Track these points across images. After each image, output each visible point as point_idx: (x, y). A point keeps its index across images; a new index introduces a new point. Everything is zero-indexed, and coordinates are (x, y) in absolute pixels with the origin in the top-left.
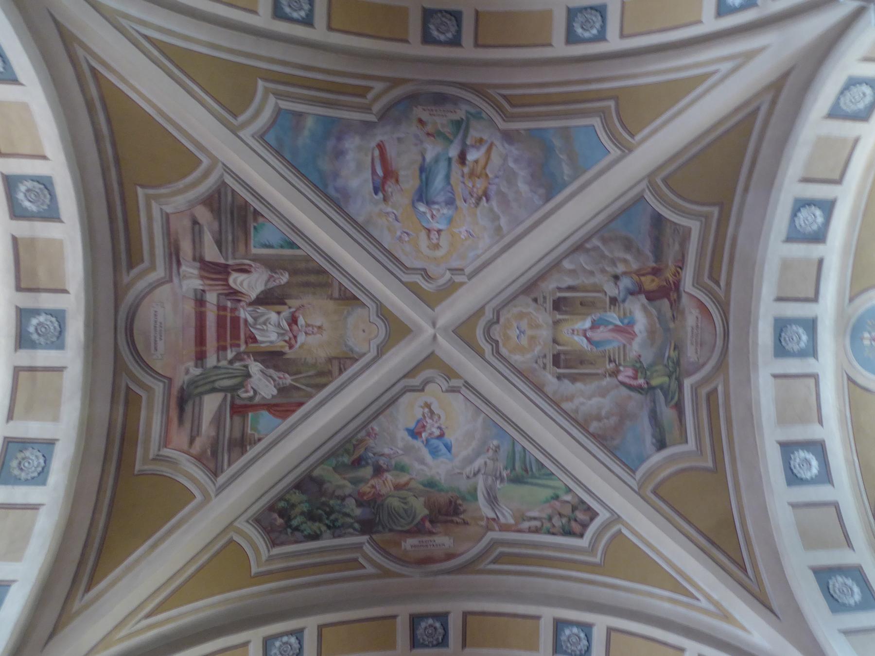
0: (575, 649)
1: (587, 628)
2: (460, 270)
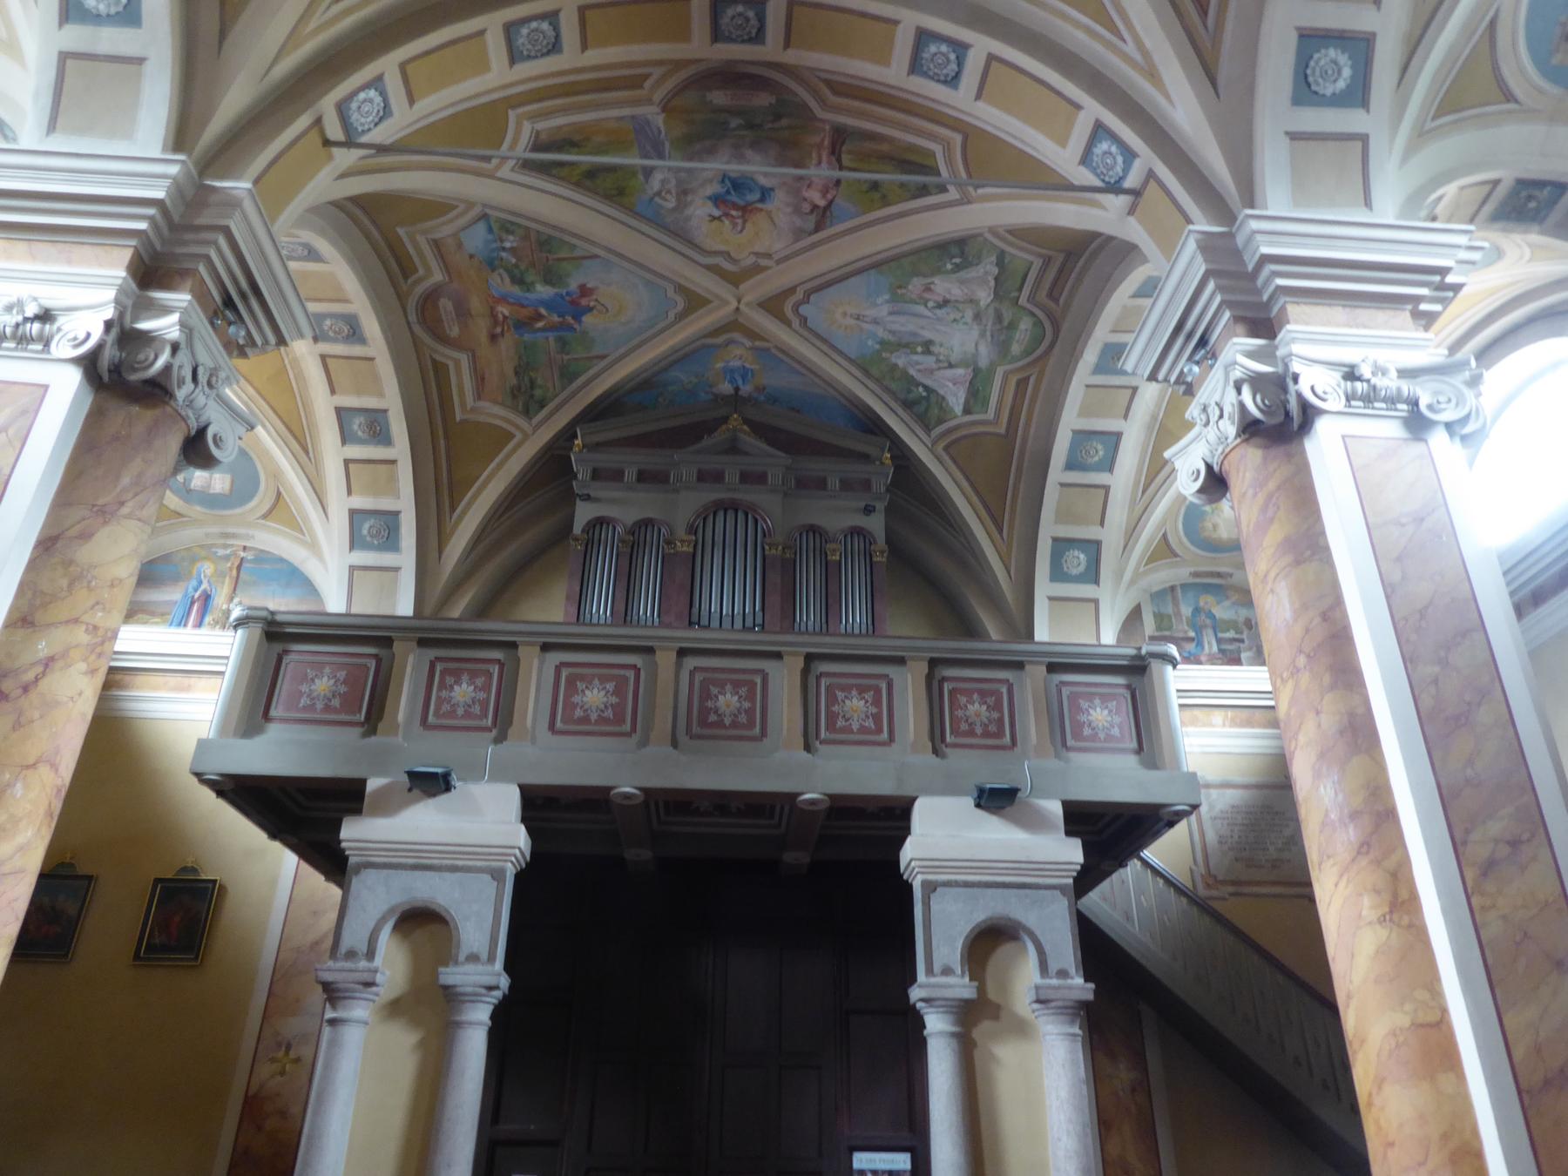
0: (939, 72)
1: (961, 48)
2: (768, 256)
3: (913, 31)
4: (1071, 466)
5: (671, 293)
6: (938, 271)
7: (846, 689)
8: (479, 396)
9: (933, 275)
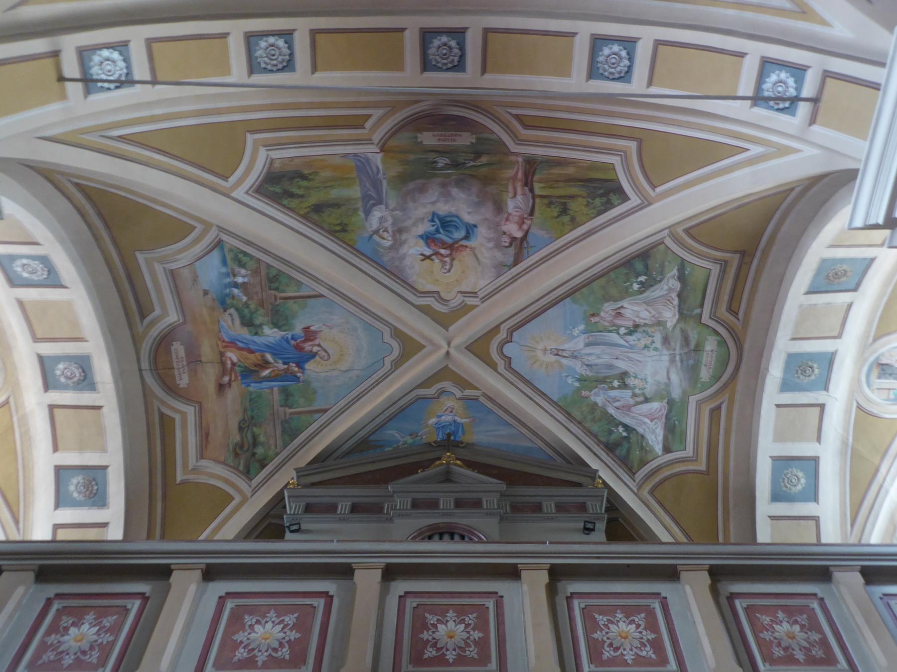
2: (473, 294)
3: (589, 37)
4: (777, 496)
5: (387, 338)
6: (626, 293)
7: (609, 611)
8: (202, 456)
9: (621, 299)
